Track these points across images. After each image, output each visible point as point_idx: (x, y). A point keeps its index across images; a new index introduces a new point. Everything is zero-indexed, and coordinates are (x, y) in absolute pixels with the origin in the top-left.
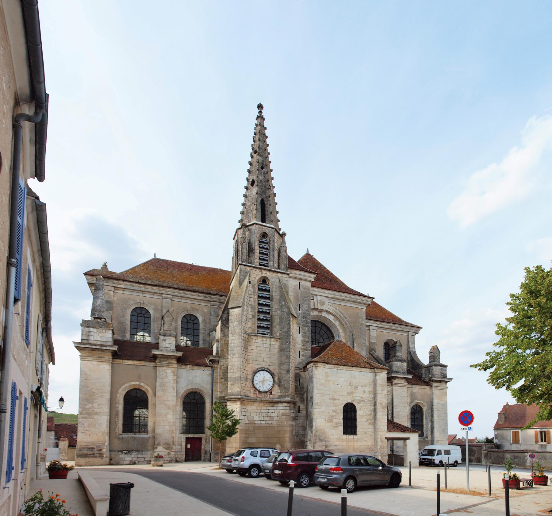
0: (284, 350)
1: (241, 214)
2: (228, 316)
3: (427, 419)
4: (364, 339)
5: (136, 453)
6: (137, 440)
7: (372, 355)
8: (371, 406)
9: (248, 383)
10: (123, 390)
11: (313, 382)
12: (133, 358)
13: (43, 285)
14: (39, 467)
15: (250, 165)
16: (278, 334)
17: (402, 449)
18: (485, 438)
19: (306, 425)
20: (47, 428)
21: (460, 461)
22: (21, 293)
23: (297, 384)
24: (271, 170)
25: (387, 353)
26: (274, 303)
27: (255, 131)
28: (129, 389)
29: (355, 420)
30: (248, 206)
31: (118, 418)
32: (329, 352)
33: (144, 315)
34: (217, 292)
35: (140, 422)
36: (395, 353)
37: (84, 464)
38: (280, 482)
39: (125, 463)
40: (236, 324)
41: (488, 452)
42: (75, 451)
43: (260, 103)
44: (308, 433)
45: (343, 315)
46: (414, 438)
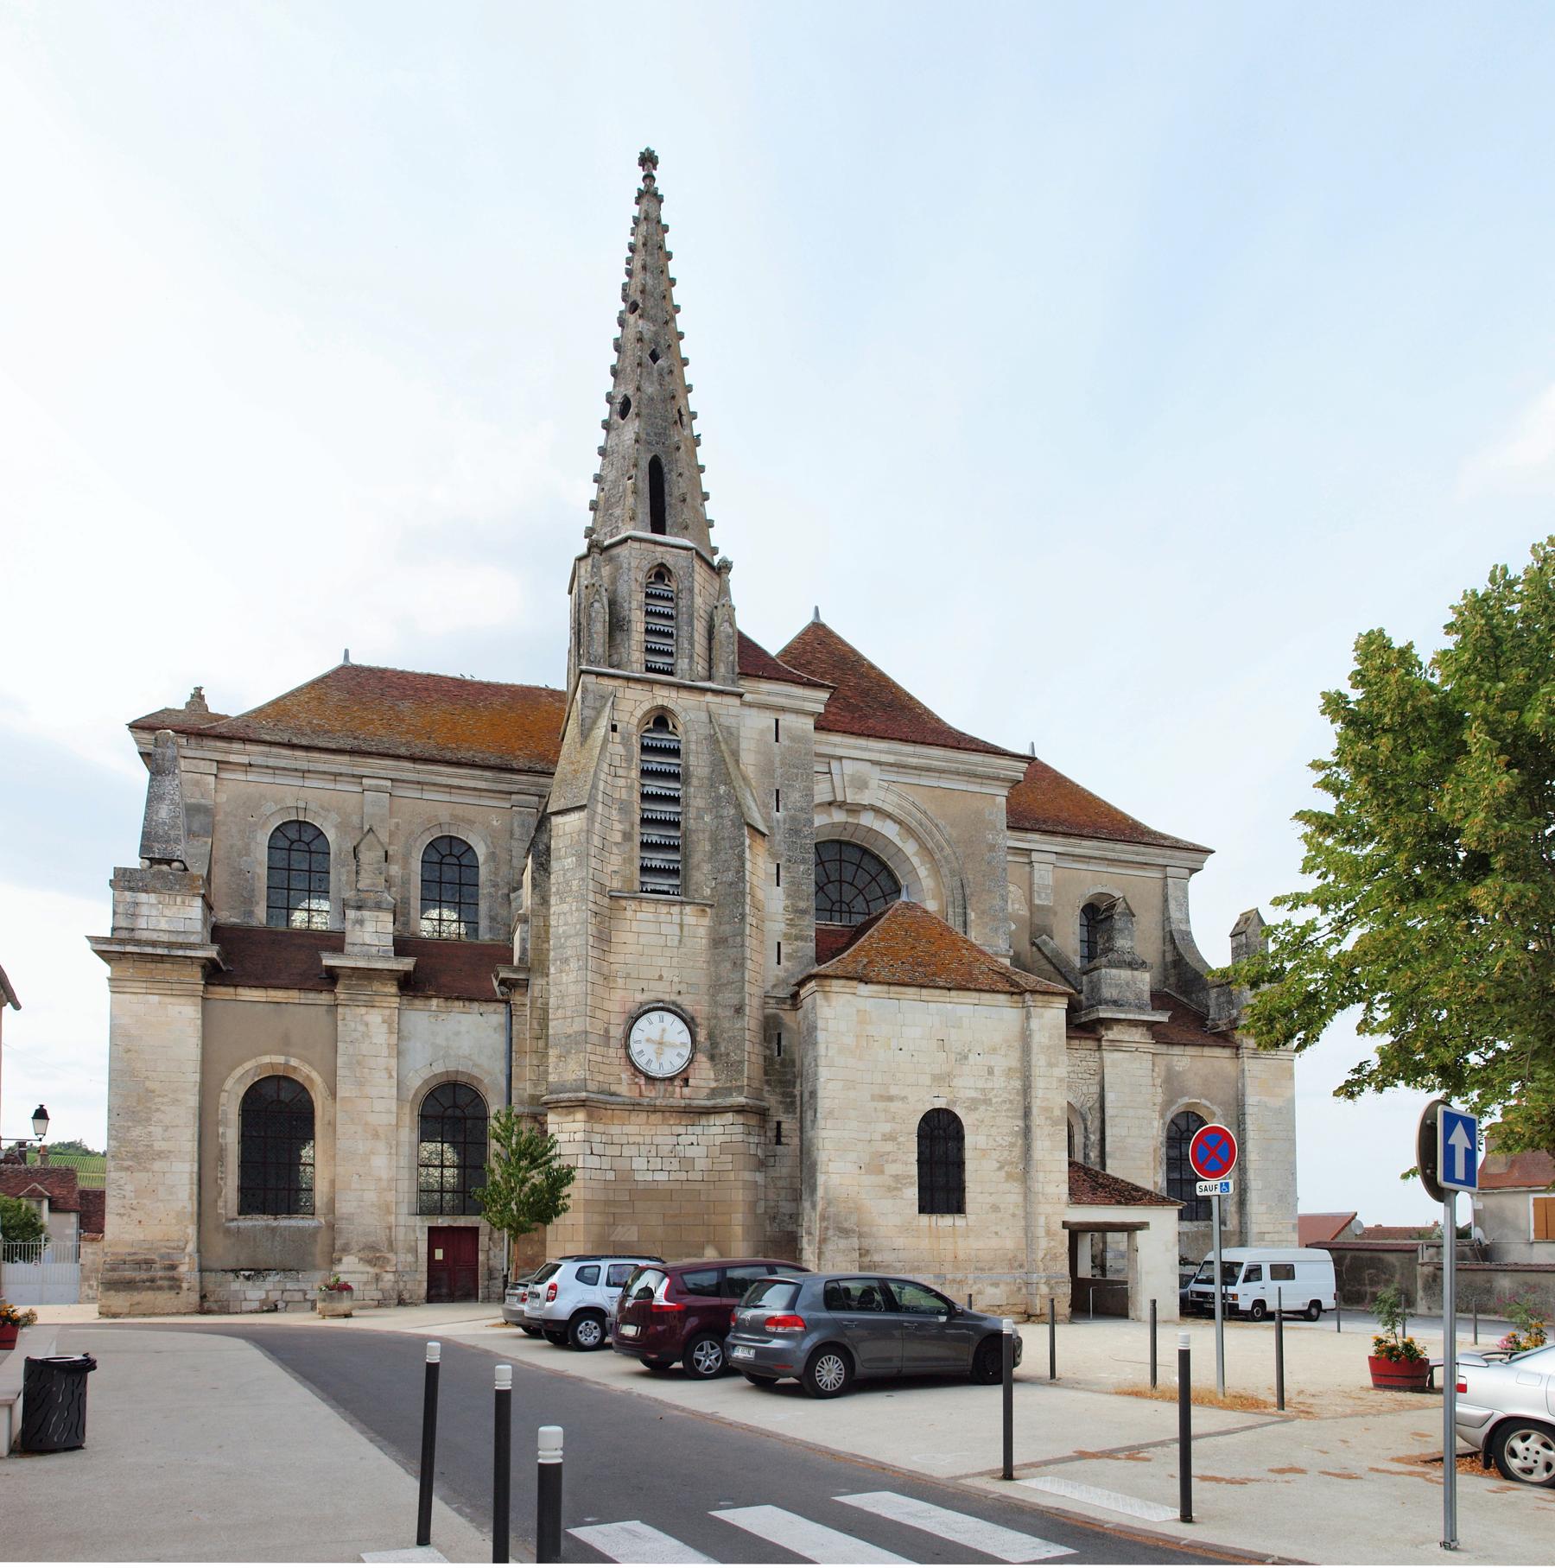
0: (726, 940)
5: (277, 1278)
7: (1039, 949)
8: (1012, 1118)
9: (612, 1052)
11: (815, 1043)
12: (267, 982)
16: (708, 892)
21: (1328, 1302)
24: (685, 362)
26: (692, 789)
27: (632, 239)
28: (256, 1079)
29: (961, 1164)
31: (223, 1169)
32: (871, 944)
33: (308, 844)
36: (1110, 939)
37: (126, 1310)
39: (246, 1306)
40: (570, 862)
43: (647, 149)
45: (931, 820)
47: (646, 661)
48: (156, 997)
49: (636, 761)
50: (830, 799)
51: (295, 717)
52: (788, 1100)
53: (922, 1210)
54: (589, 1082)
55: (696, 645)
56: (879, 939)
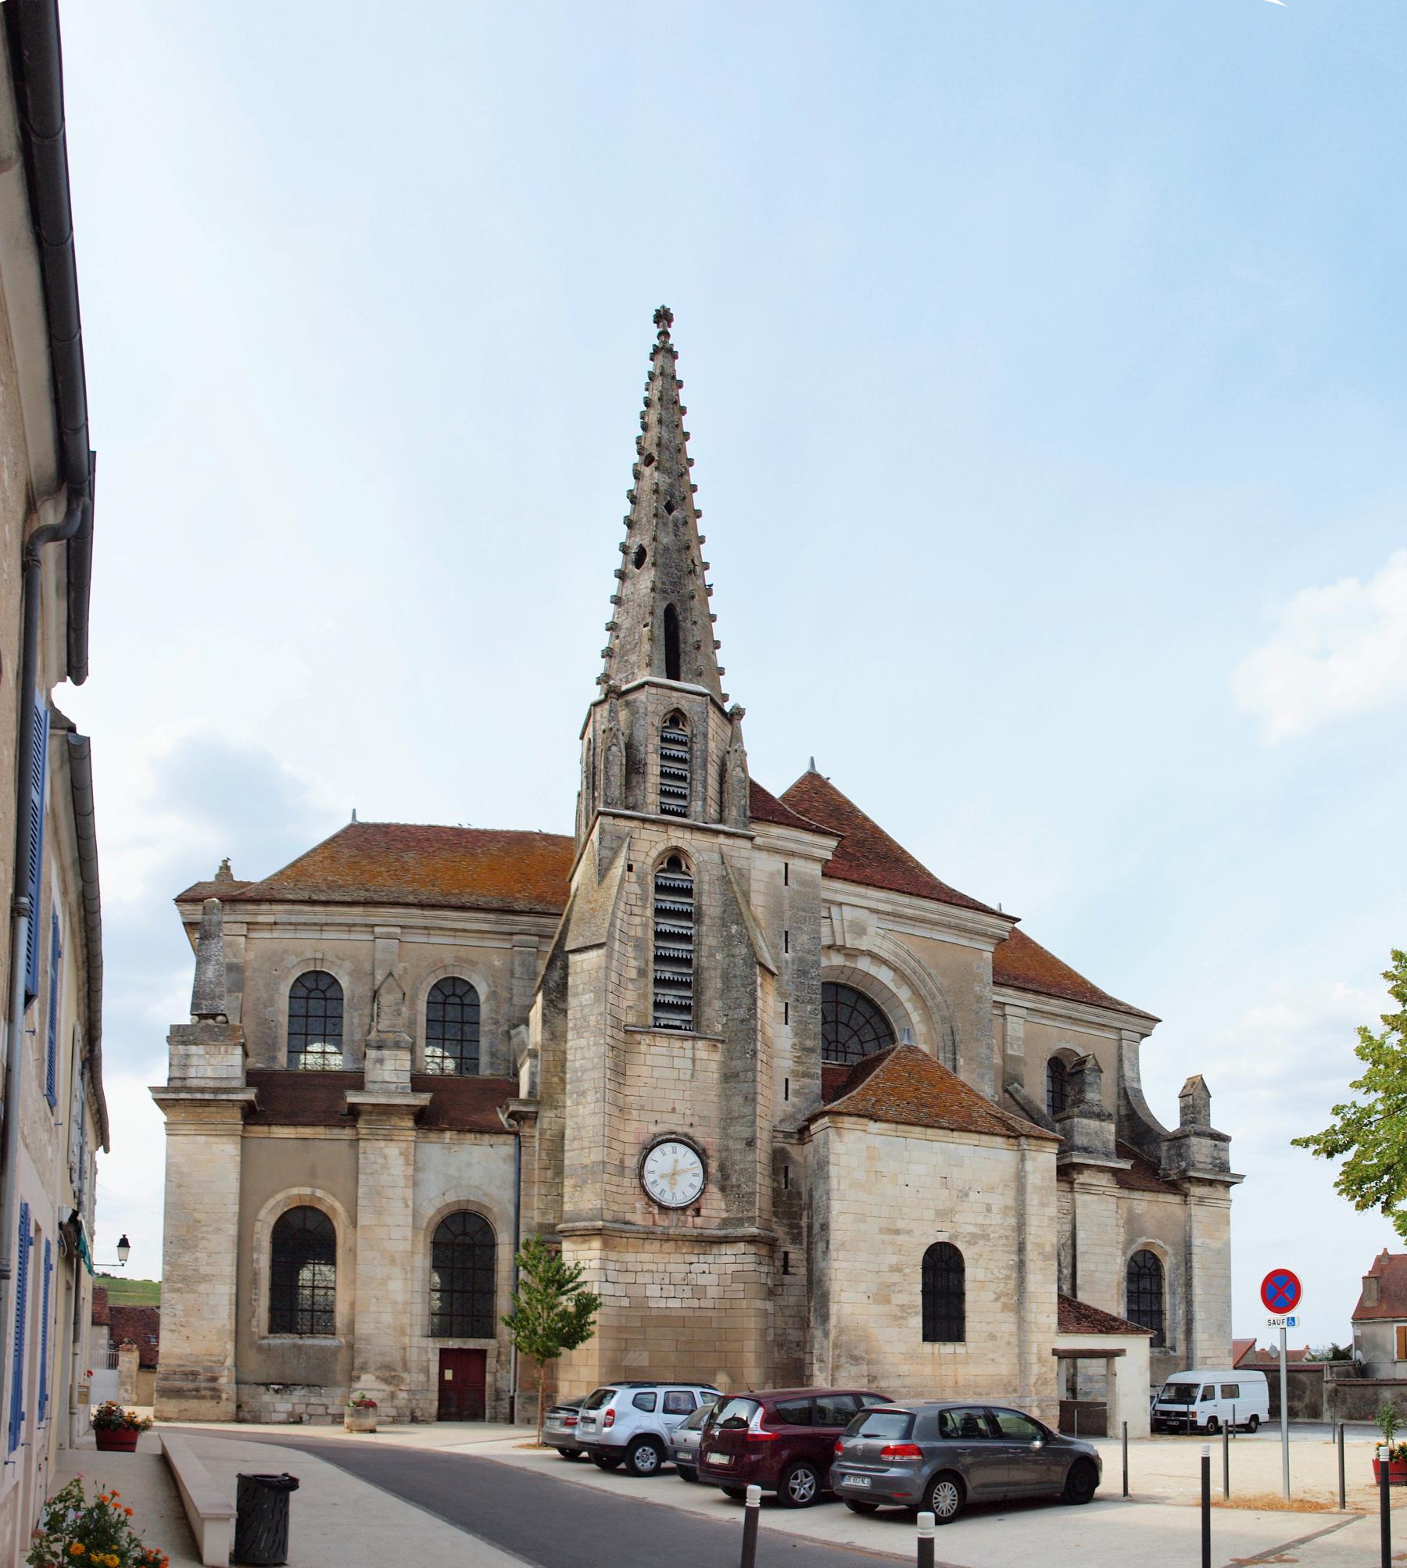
0: (737, 1075)
1: (603, 657)
2: (566, 975)
3: (1173, 1293)
4: (988, 1044)
6: (306, 1353)
7: (1011, 1095)
8: (1008, 1252)
9: (626, 1182)
10: (271, 1211)
11: (827, 1178)
12: (296, 1120)
13: (85, 949)
14: (76, 1417)
15: (632, 502)
17: (1101, 1385)
18: (1331, 1346)
19: (809, 1313)
20: (93, 1316)
21: (1264, 1416)
22: (40, 979)
23: (779, 1182)
24: (698, 514)
25: (1056, 1090)
26: (705, 928)
27: (646, 394)
28: (285, 1210)
29: (960, 1295)
30: (627, 629)
31: (257, 1291)
32: (877, 1084)
34: (531, 903)
35: (313, 1303)
36: (1081, 1091)
37: (175, 1416)
38: (727, 1490)
39: (275, 1417)
40: (588, 998)
41: (1339, 1388)
42: (154, 1380)
43: (663, 307)
44: (813, 1337)
46: (1137, 1349)
47: (661, 803)
48: (204, 1137)
49: (651, 899)
50: (830, 943)
51: (312, 875)
52: (795, 1231)
53: (926, 1338)
54: (605, 1211)
55: (709, 788)
56: (885, 1079)
